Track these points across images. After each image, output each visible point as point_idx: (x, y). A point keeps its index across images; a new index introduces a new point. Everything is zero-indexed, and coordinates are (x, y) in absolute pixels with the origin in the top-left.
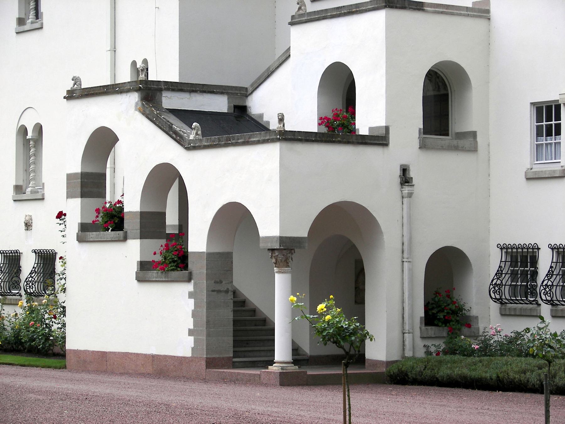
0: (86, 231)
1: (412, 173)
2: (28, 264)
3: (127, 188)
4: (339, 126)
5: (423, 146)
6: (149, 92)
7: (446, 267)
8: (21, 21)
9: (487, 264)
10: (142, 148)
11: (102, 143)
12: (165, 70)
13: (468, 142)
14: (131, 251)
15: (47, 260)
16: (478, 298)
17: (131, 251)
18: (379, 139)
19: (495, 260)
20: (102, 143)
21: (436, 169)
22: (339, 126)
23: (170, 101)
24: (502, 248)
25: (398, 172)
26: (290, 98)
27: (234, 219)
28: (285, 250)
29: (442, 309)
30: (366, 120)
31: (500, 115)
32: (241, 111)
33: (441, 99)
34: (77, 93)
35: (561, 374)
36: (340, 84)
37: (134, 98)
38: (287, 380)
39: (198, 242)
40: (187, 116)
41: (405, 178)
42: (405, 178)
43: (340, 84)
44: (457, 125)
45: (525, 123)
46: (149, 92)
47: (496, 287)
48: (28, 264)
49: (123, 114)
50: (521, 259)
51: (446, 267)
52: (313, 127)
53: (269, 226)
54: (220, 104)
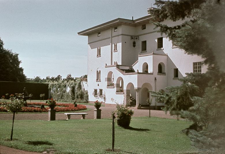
1: (157, 79)
2: (98, 91)
4: (146, 71)
5: (158, 75)
8: (98, 55)
11: (110, 73)
23: (121, 67)
25: (154, 78)
41: (155, 79)
42: (155, 79)
44: (152, 73)
48: (98, 91)
49: (114, 70)
53: (136, 86)
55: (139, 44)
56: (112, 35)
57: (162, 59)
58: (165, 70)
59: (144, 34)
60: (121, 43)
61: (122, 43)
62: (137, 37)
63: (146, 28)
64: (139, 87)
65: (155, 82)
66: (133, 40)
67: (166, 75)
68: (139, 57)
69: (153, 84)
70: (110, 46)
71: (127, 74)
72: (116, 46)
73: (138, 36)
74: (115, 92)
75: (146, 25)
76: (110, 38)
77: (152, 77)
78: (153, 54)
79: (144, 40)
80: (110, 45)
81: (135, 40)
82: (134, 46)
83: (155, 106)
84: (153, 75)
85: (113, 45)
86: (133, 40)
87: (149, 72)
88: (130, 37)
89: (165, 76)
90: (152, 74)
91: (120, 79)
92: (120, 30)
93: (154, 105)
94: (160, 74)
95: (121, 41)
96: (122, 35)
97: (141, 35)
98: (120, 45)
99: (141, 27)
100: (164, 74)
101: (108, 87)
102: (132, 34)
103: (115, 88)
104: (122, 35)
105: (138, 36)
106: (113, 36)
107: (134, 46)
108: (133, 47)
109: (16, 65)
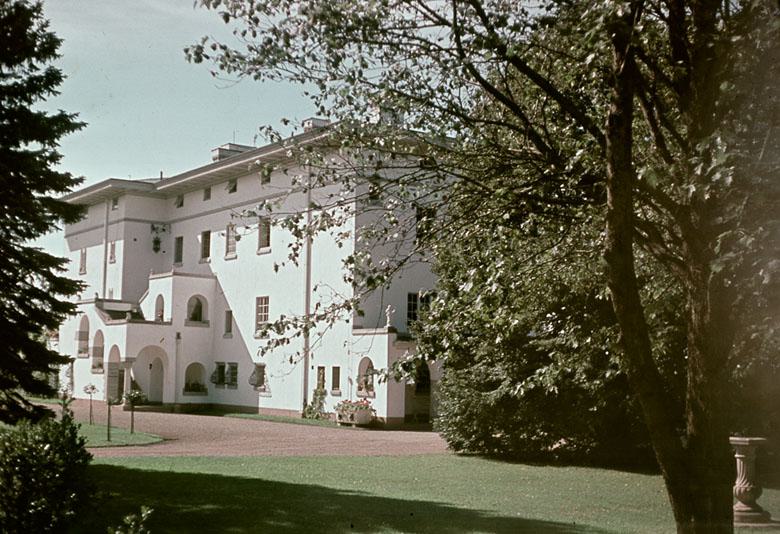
4: (159, 320)
5: (186, 325)
12: (118, 296)
14: (90, 361)
22: (159, 320)
23: (107, 306)
24: (218, 363)
25: (175, 335)
26: (148, 311)
30: (167, 317)
41: (178, 336)
42: (178, 336)
52: (153, 319)
53: (123, 355)
55: (169, 244)
56: (107, 218)
57: (200, 287)
58: (209, 314)
60: (122, 242)
61: (125, 243)
62: (166, 226)
63: (185, 203)
64: (130, 356)
65: (177, 344)
66: (154, 235)
67: (209, 326)
68: (151, 282)
69: (170, 349)
70: (103, 247)
71: (117, 321)
72: (113, 246)
73: (169, 224)
74: (91, 367)
75: (238, 180)
76: (102, 226)
77: (169, 333)
78: (175, 274)
79: (180, 235)
80: (102, 243)
81: (161, 235)
82: (156, 249)
83: (175, 404)
84: (173, 326)
85: (109, 245)
86: (154, 235)
87: (165, 320)
88: (149, 225)
89: (206, 330)
90: (170, 324)
91: (100, 333)
92: (122, 209)
93: (173, 401)
94: (194, 323)
95: (122, 236)
96: (125, 220)
97: (174, 221)
98: (120, 245)
99: (175, 200)
100: (207, 323)
101: (96, 370)
102: (154, 217)
103: (91, 358)
104: (125, 220)
105: (169, 224)
106: (110, 221)
107: (156, 249)
108: (153, 252)
109: (774, 99)
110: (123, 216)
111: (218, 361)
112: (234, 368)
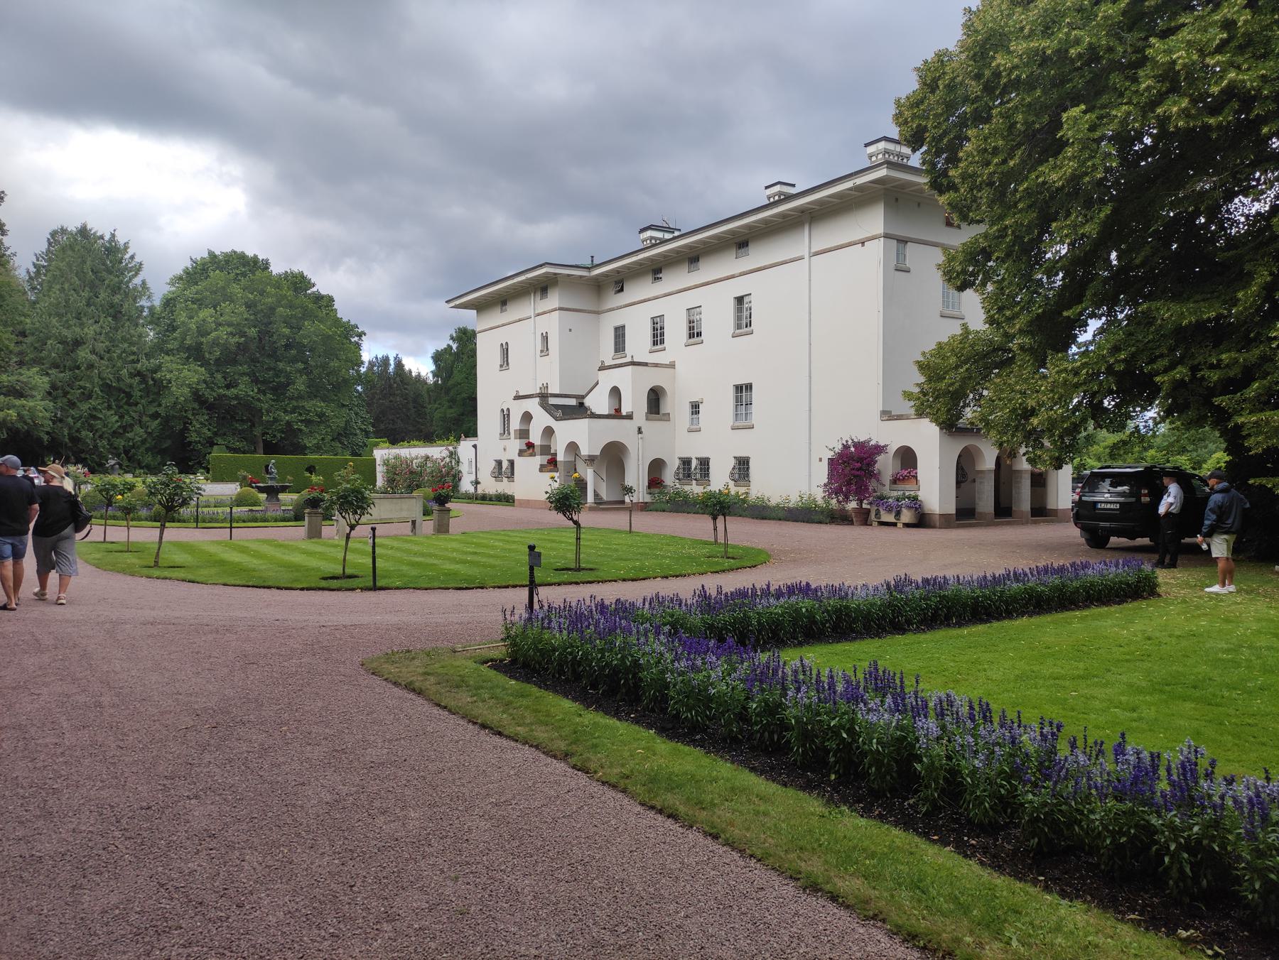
0: (521, 453)
2: (505, 465)
3: (536, 437)
6: (543, 397)
7: (657, 466)
9: (673, 465)
10: (542, 420)
11: (527, 417)
12: (554, 389)
13: (667, 417)
14: (538, 460)
15: (512, 463)
16: (669, 478)
17: (538, 460)
18: (629, 417)
19: (677, 463)
20: (527, 417)
21: (652, 427)
23: (552, 401)
26: (598, 402)
27: (573, 447)
28: (591, 460)
29: (655, 482)
31: (676, 405)
32: (582, 404)
33: (655, 399)
34: (517, 398)
35: (1225, 12)
36: (616, 392)
37: (537, 400)
38: (591, 509)
39: (560, 458)
40: (557, 407)
43: (616, 392)
44: (662, 411)
45: (688, 409)
46: (543, 397)
47: (677, 474)
48: (505, 465)
49: (533, 406)
50: (686, 462)
51: (657, 466)
53: (585, 451)
54: (573, 402)
59: (613, 309)
76: (801, 258)
92: (554, 300)
110: (557, 306)
111: (738, 455)
112: (705, 463)
